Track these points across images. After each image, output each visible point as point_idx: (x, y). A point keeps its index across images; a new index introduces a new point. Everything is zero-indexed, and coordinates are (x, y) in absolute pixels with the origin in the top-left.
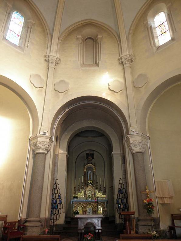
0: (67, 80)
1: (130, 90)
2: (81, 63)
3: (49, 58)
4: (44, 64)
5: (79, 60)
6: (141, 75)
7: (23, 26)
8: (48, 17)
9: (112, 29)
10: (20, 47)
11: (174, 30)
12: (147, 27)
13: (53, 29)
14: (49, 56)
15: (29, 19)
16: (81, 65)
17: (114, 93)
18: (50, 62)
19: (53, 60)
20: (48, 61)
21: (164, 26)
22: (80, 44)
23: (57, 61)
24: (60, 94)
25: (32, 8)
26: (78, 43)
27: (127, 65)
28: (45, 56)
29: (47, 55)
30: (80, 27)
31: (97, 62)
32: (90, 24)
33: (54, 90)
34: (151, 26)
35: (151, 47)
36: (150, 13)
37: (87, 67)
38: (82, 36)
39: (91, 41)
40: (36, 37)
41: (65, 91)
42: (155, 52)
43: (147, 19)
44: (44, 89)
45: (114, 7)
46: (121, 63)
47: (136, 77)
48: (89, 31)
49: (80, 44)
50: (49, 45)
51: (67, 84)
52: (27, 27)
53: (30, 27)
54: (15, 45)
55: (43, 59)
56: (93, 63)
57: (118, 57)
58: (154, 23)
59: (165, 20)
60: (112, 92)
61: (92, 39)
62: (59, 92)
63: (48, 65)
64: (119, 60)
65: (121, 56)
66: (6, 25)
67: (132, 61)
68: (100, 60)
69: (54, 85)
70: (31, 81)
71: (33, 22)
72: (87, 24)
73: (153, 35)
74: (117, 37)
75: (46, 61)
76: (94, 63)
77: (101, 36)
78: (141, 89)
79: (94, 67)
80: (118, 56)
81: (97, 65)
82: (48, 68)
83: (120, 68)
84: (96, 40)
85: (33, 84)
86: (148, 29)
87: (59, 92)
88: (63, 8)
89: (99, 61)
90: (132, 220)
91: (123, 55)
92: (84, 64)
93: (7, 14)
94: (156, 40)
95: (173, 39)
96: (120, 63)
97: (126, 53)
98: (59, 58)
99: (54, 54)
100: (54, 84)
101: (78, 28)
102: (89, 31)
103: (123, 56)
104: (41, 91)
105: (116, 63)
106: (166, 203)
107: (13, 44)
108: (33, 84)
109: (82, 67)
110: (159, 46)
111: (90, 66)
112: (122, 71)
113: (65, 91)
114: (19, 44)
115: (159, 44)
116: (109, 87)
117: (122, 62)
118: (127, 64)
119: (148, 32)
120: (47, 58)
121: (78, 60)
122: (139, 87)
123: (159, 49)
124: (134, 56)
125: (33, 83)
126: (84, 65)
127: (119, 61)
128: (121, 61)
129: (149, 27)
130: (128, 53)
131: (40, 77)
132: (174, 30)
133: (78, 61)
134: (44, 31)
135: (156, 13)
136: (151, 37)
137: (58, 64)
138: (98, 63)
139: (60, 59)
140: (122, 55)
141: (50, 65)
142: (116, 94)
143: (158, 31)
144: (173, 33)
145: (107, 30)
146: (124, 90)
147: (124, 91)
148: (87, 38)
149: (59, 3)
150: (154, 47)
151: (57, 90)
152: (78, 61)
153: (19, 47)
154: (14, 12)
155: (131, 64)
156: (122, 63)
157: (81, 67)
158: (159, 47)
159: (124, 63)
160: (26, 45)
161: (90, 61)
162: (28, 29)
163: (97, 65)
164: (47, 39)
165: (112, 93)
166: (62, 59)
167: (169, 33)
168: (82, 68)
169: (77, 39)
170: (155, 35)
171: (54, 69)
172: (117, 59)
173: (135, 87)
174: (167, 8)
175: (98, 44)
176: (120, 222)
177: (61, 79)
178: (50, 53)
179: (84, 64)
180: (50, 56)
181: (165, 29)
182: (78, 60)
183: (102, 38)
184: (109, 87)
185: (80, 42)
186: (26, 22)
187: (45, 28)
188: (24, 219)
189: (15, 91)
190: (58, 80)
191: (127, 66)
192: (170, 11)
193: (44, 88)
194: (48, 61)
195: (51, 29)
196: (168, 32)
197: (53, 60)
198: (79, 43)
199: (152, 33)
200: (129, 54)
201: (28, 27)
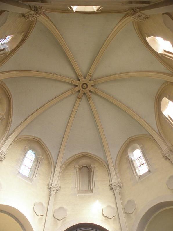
0: (65, 207)
1: (123, 217)
2: (78, 189)
3: (51, 185)
4: (47, 191)
5: (77, 187)
6: (129, 201)
7: (34, 161)
8: (53, 153)
9: (102, 159)
10: (30, 179)
11: (149, 164)
12: (129, 160)
14: (51, 184)
15: (39, 155)
16: (78, 191)
17: (108, 219)
18: (52, 189)
19: (54, 188)
20: (50, 189)
22: (77, 172)
23: (58, 188)
24: (58, 221)
25: (42, 147)
26: (76, 171)
27: (117, 191)
28: (48, 184)
29: (50, 183)
30: (78, 158)
31: (92, 188)
32: (85, 156)
33: (53, 217)
34: (132, 159)
35: (134, 176)
36: (129, 149)
37: (83, 193)
38: (79, 166)
39: (86, 169)
40: (43, 168)
41: (64, 218)
42: (138, 180)
43: (128, 154)
44: (44, 217)
45: (102, 144)
46: (111, 189)
47: (126, 202)
48: (84, 162)
49: (77, 172)
50: (52, 175)
51: (65, 210)
52: (37, 161)
53: (39, 161)
54: (25, 177)
55: (46, 187)
56: (88, 189)
57: (109, 184)
58: (133, 157)
59: (141, 155)
60: (106, 218)
61: (87, 167)
62: (58, 219)
63: (50, 192)
64: (109, 186)
65: (111, 183)
66: (22, 162)
67: (120, 187)
68: (94, 186)
69: (54, 212)
70: (35, 211)
72: (83, 156)
73: (134, 166)
74: (107, 167)
75: (49, 189)
76: (89, 189)
77: (94, 166)
78: (131, 215)
79: (88, 193)
80: (109, 183)
81: (92, 191)
82: (50, 195)
83: (111, 193)
84: (90, 169)
85: (35, 212)
86: (129, 161)
87: (58, 219)
89: (93, 187)
91: (113, 182)
92: (80, 190)
94: (137, 170)
95: (149, 171)
96: (110, 189)
97: (115, 180)
98: (60, 185)
99: (56, 183)
100: (53, 211)
102: (84, 162)
103: (113, 183)
104: (42, 218)
105: (108, 188)
106: (28, 151)
107: (25, 176)
108: (35, 212)
109: (78, 193)
110: (141, 175)
111: (86, 192)
112: (113, 196)
113: (64, 218)
114: (28, 176)
115: (140, 173)
116: (103, 213)
117: (112, 188)
118: (117, 190)
119: (130, 163)
120: (50, 186)
121: (76, 186)
122: (130, 213)
123: (141, 178)
124: (122, 183)
125: (36, 211)
126: (80, 191)
127: (110, 187)
128: (111, 187)
129: (130, 159)
130: (116, 181)
131: (42, 204)
132: (149, 164)
133: (76, 187)
134: (49, 163)
135: (134, 149)
136: (133, 168)
137: (58, 191)
138: (93, 189)
139: (60, 187)
140: (112, 182)
141: (52, 193)
142: (109, 220)
143: (137, 163)
144: (149, 166)
146: (117, 215)
147: (117, 217)
148: (83, 167)
149: (43, 107)
150: (136, 176)
151: (56, 217)
152: (76, 187)
153: (28, 178)
155: (120, 189)
156: (112, 189)
157: (78, 194)
158: (140, 177)
159: (114, 189)
160: (34, 176)
161: (86, 188)
162: (37, 163)
163: (92, 191)
164: (51, 169)
165: (106, 219)
166: (62, 187)
167: (146, 165)
168: (79, 194)
169: (75, 168)
170: (135, 166)
171: (55, 195)
172: (108, 185)
173: (126, 213)
174: (141, 148)
175: (92, 172)
177: (61, 205)
178: (52, 182)
179: (80, 190)
180: (52, 184)
182: (76, 186)
183: (94, 167)
184: (103, 213)
185: (77, 171)
186: (37, 157)
187: (50, 161)
189: (19, 221)
190: (57, 207)
191: (117, 192)
192: (143, 150)
193: (45, 215)
194: (50, 189)
195: (55, 162)
196: (145, 164)
197: (54, 188)
198: (76, 172)
199: (133, 164)
200: (117, 181)
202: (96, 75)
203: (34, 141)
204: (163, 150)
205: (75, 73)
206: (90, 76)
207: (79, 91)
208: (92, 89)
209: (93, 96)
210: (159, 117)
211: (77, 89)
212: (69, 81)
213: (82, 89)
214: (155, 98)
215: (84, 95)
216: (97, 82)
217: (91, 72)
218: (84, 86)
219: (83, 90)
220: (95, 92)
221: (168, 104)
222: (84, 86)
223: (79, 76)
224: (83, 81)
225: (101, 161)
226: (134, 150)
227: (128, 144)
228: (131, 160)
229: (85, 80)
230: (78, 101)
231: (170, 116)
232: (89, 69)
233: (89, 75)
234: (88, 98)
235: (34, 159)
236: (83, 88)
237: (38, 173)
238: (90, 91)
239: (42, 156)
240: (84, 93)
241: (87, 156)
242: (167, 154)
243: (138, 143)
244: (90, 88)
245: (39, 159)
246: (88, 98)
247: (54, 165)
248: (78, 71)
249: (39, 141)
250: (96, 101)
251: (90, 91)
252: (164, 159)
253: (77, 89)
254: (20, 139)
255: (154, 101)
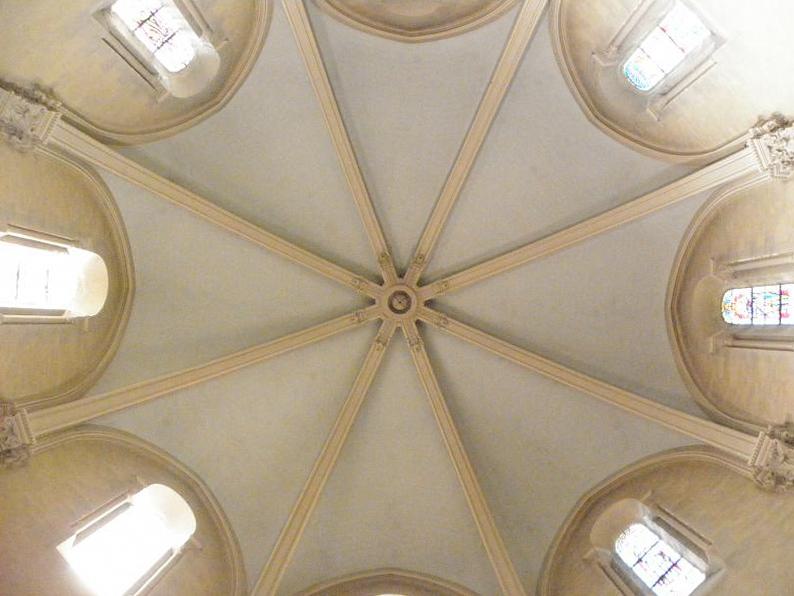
8: (547, 58)
9: (335, 18)
13: (540, 22)
21: (154, 38)
30: (443, 23)
34: (199, 32)
36: (214, 68)
45: (332, 79)
53: (614, 49)
71: (597, 59)
74: (115, 136)
86: (208, 27)
88: (491, 86)
90: (765, 279)
93: (669, 96)
101: (451, 20)
134: (570, 26)
145: (350, 12)
154: (647, 89)
176: (702, 572)
181: (148, 31)
188: (596, 84)
195: (544, 27)
201: (619, 47)
202: (358, 341)
203: (620, 125)
204: (28, 416)
205: (430, 351)
206: (378, 341)
207: (421, 283)
208: (372, 314)
209: (368, 260)
210: (107, 229)
211: (428, 292)
212: (454, 280)
213: (409, 292)
214: (134, 288)
215: (405, 263)
216: (356, 319)
217: (376, 356)
218: (400, 303)
219: (404, 289)
220: (357, 315)
221: (80, 285)
222: (400, 303)
223: (418, 343)
224: (405, 322)
225: (340, 11)
226: (191, 63)
227: (222, 86)
228: (201, 30)
229: (399, 325)
230: (426, 247)
231: (62, 254)
232: (381, 369)
233: (384, 344)
234: (388, 254)
235: (631, 54)
236: (404, 294)
237: (629, 12)
238: (381, 282)
239: (594, 63)
240: (401, 276)
241: (401, 27)
242: (35, 117)
243: (181, 101)
244: (383, 295)
245: (610, 55)
246: (388, 254)
247: (552, 11)
248: (422, 358)
249: (596, 116)
250: (358, 244)
251: (381, 282)
252: (47, 82)
253: (428, 292)
254: (672, 149)
255: (137, 276)
